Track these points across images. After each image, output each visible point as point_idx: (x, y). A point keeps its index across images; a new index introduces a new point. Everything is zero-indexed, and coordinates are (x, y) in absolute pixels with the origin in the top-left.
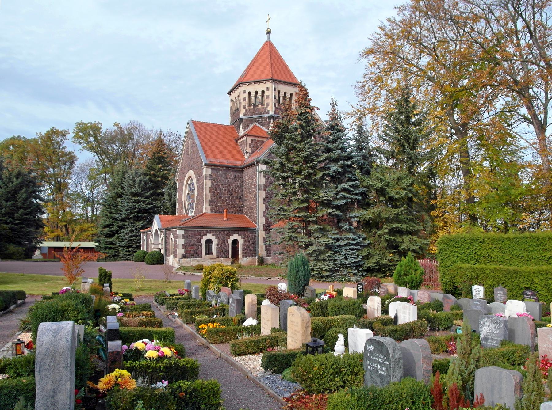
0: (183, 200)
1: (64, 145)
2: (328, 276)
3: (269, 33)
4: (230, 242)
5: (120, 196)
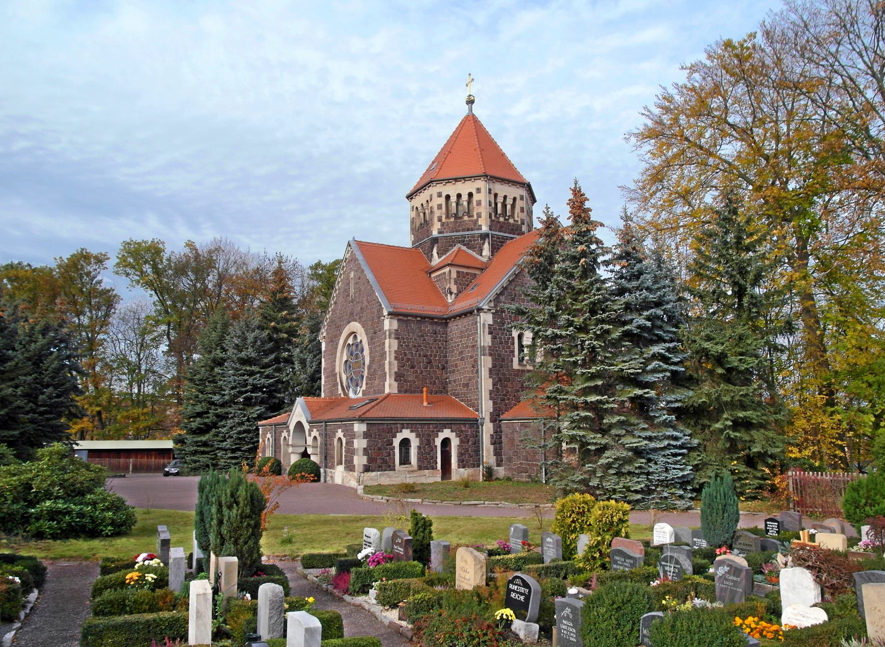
0: (337, 370)
1: (99, 278)
2: (638, 501)
3: (470, 102)
4: (438, 442)
5: (220, 363)
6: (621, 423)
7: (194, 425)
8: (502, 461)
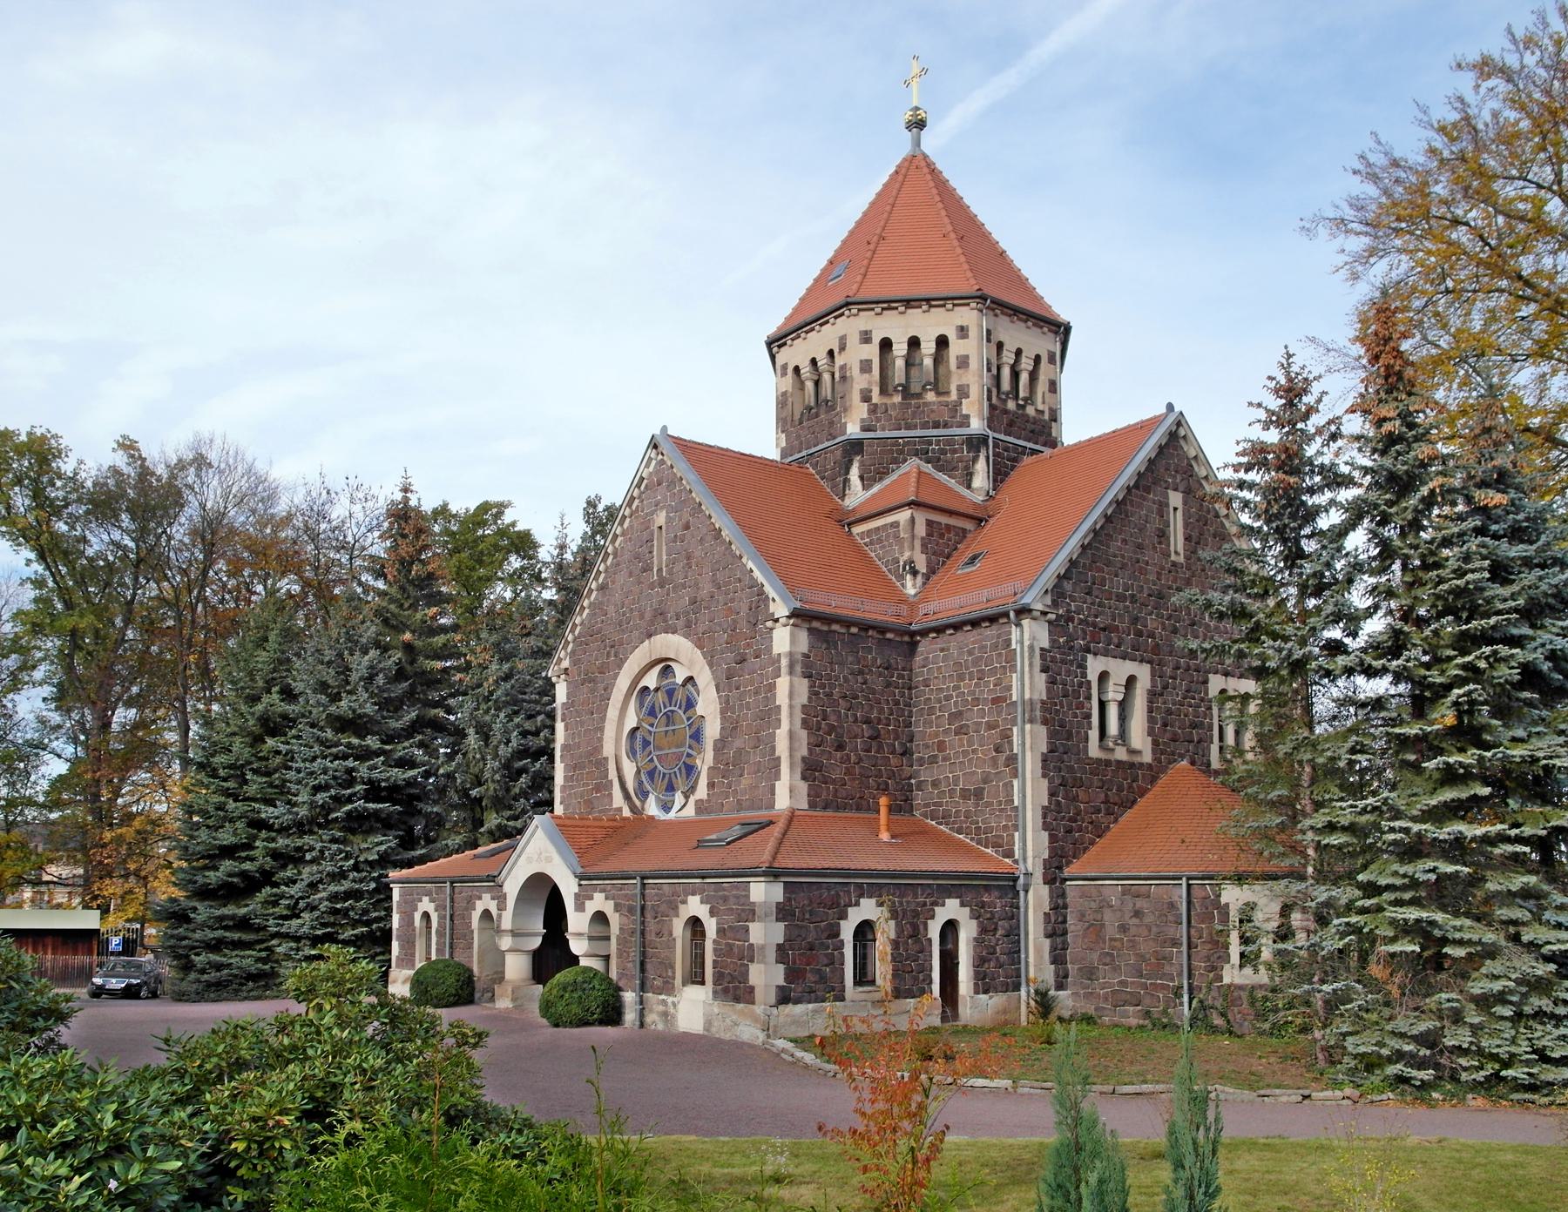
0: (608, 749)
3: (918, 125)
5: (273, 726)
6: (1526, 894)
7: (213, 877)
8: (1066, 976)
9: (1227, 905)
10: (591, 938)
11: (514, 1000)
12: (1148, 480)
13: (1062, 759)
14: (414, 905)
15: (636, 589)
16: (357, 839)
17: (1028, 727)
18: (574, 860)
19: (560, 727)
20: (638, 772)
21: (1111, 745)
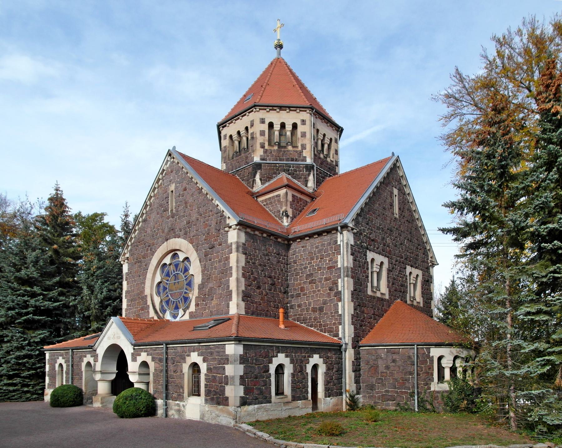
0: (147, 292)
8: (360, 389)
9: (433, 357)
10: (140, 374)
11: (102, 403)
12: (387, 182)
13: (358, 294)
14: (57, 363)
15: (160, 220)
16: (30, 332)
17: (346, 279)
18: (131, 337)
19: (125, 283)
20: (161, 301)
21: (375, 290)
